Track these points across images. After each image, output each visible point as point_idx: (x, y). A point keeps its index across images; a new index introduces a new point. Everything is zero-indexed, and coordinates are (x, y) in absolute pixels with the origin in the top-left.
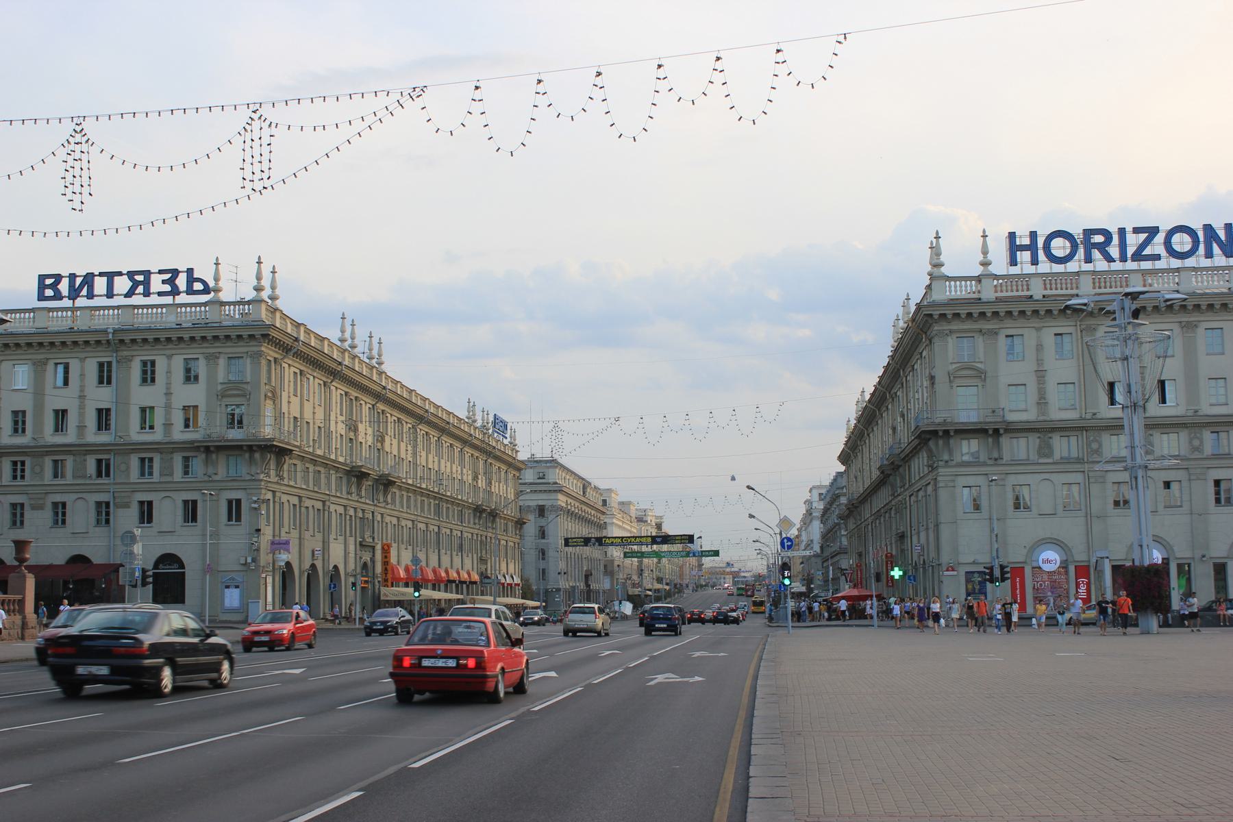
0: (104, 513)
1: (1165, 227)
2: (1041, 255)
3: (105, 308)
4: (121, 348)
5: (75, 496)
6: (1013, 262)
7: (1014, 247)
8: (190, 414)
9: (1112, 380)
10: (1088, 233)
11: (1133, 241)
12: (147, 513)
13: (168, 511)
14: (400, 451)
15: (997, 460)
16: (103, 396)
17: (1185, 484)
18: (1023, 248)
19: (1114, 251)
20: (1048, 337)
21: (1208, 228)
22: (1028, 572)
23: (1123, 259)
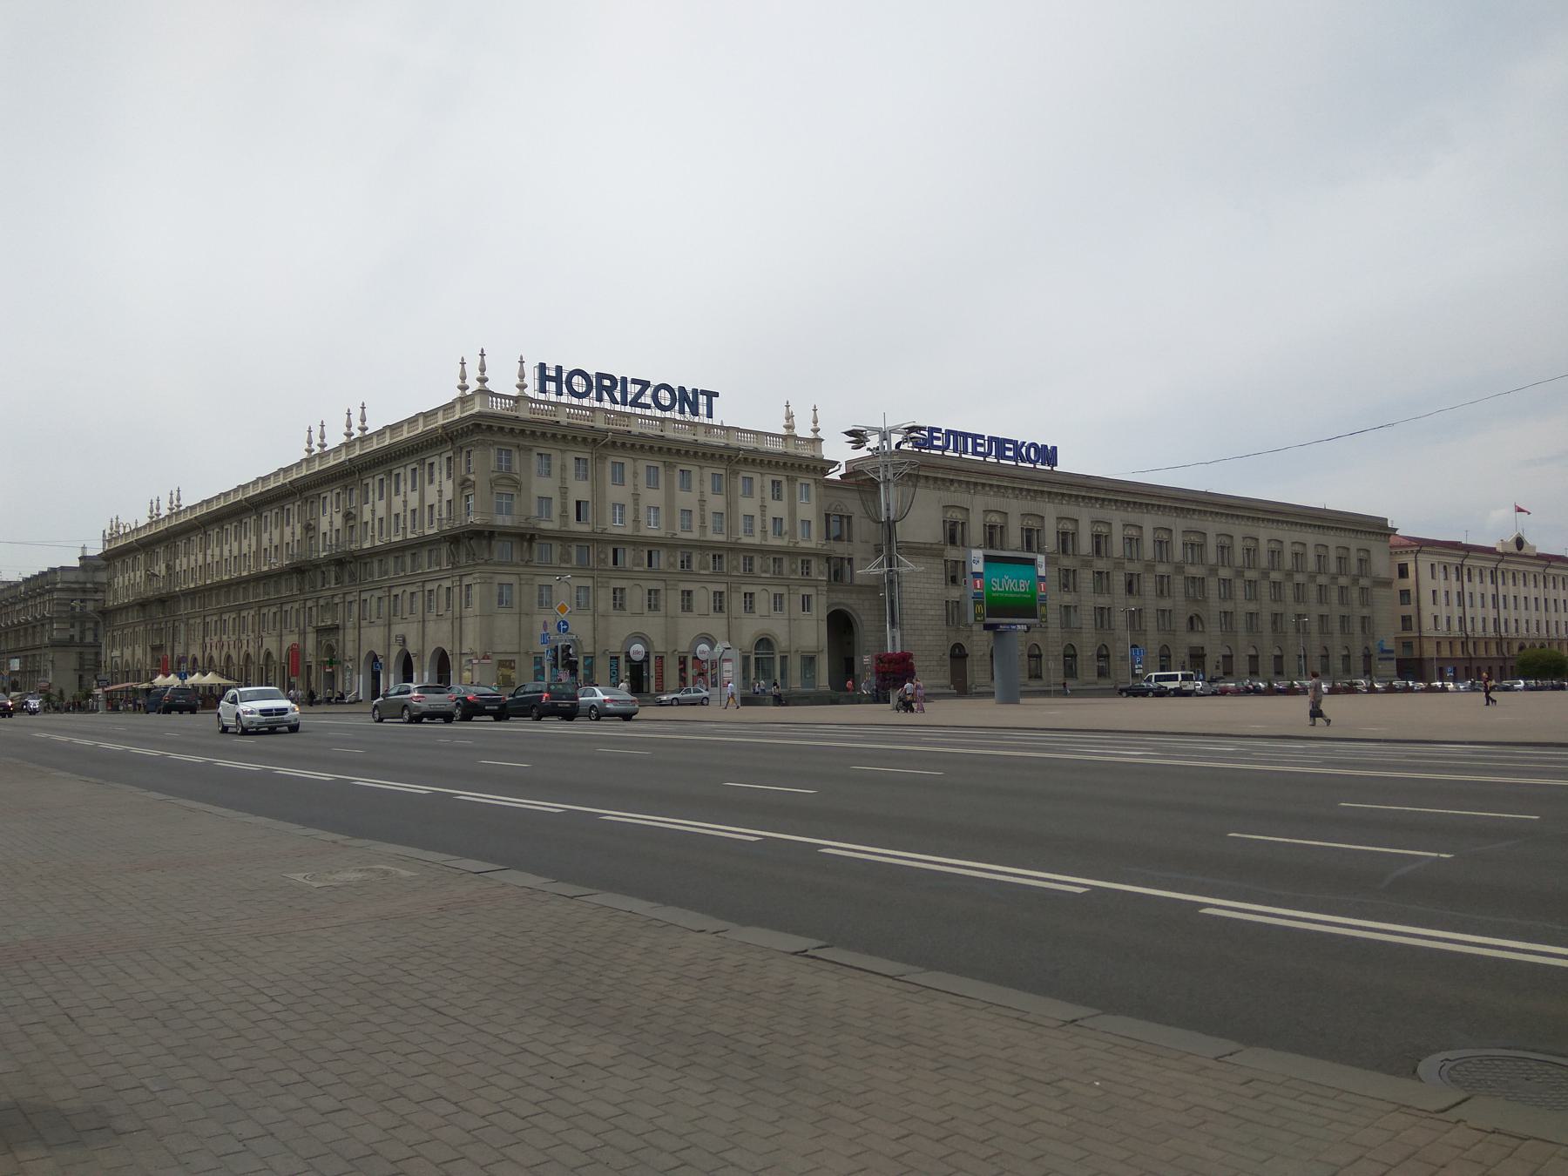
1: (655, 382)
2: (565, 390)
4: (600, 445)
5: (631, 583)
6: (543, 390)
7: (543, 378)
10: (601, 376)
11: (633, 389)
13: (763, 602)
15: (527, 563)
17: (516, 587)
18: (551, 379)
19: (618, 395)
20: (708, 472)
21: (682, 389)
23: (624, 403)
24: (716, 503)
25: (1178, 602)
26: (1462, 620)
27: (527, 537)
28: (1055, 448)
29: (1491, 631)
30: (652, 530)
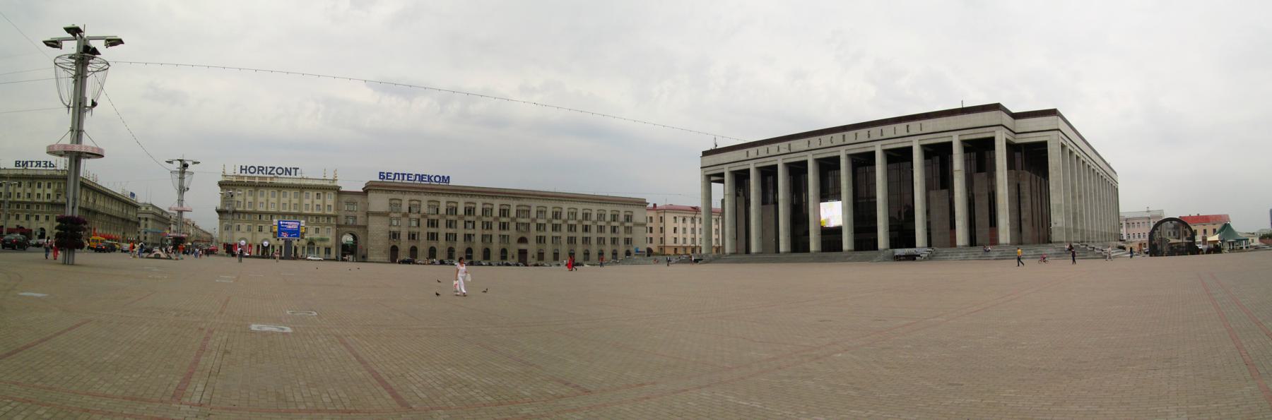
0: (28, 218)
3: (32, 170)
8: (49, 195)
9: (973, 249)
12: (37, 218)
13: (42, 218)
14: (101, 204)
16: (29, 190)
22: (1054, 158)
24: (295, 201)
25: (608, 235)
26: (694, 240)
27: (235, 212)
28: (221, 184)
29: (689, 243)
30: (272, 210)
